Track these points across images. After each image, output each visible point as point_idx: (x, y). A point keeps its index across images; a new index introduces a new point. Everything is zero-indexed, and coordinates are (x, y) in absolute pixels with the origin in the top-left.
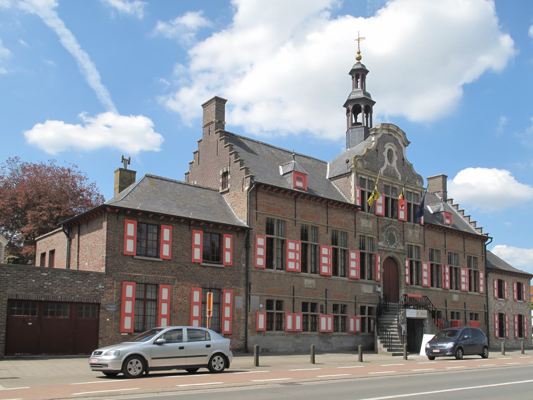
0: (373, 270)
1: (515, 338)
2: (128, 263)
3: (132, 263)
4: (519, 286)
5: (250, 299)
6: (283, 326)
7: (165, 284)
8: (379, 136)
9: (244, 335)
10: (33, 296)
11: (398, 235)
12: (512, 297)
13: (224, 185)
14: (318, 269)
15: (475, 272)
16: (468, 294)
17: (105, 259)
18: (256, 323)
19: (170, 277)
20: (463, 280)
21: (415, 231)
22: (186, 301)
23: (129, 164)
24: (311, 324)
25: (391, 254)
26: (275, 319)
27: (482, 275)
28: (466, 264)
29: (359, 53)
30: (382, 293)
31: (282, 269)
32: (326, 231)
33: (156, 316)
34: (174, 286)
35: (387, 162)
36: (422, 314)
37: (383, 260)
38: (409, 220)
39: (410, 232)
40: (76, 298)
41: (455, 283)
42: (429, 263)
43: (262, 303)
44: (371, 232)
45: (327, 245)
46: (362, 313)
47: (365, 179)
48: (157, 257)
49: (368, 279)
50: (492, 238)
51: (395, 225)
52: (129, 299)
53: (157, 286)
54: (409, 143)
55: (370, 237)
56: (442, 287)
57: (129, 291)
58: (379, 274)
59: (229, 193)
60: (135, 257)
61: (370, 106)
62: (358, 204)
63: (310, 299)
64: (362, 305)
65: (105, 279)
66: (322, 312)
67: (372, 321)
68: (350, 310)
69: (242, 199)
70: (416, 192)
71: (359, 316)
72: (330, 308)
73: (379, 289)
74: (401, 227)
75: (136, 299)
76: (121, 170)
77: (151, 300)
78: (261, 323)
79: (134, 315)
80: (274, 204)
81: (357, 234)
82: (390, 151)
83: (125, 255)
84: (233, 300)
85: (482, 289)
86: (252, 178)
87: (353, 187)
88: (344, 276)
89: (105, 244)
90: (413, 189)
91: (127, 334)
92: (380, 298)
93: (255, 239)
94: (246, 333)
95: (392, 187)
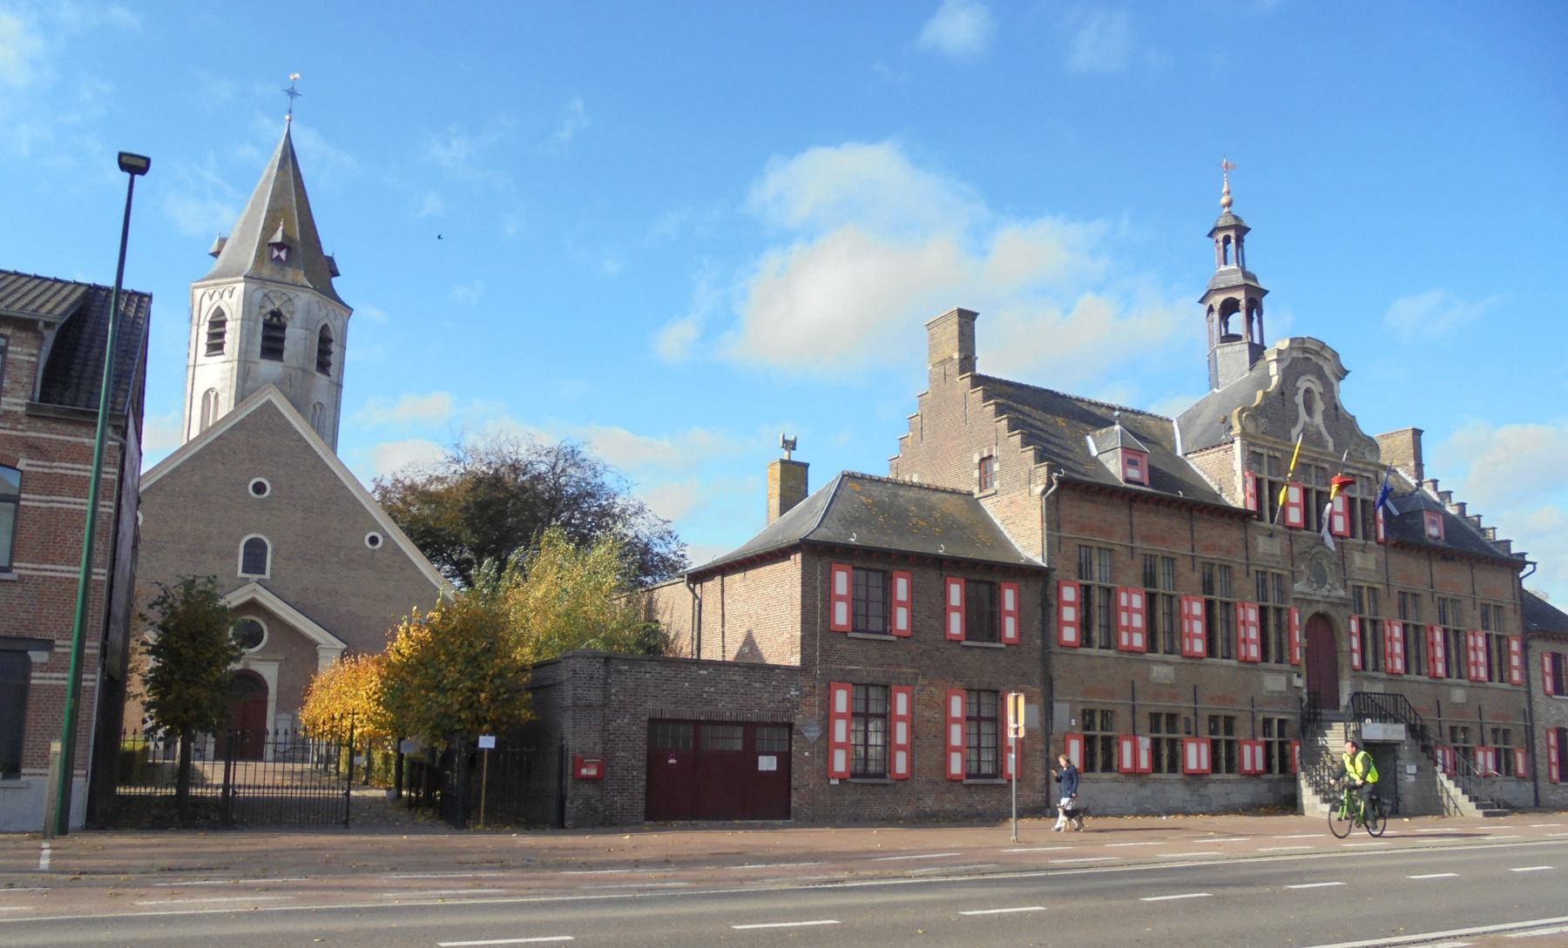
0: (1285, 641)
8: (1286, 363)
10: (686, 714)
14: (1177, 643)
24: (1167, 757)
25: (1321, 608)
27: (1515, 646)
37: (1305, 622)
39: (1358, 559)
42: (1401, 622)
53: (886, 687)
54: (1346, 372)
57: (841, 701)
63: (1165, 705)
66: (1188, 733)
68: (1242, 731)
71: (1261, 739)
76: (783, 462)
77: (877, 716)
81: (1253, 568)
82: (1308, 391)
85: (1516, 676)
87: (1239, 472)
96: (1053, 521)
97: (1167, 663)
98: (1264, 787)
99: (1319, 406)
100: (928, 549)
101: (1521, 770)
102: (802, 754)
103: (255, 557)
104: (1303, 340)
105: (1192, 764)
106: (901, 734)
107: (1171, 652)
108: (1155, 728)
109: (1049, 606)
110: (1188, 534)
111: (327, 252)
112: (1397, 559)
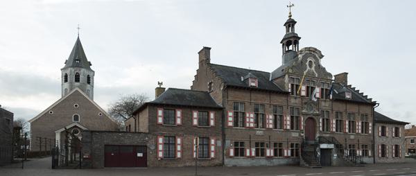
4: (397, 130)
10: (116, 144)
13: (210, 89)
15: (366, 123)
18: (229, 153)
20: (370, 128)
25: (310, 116)
27: (370, 125)
36: (332, 146)
38: (322, 97)
40: (135, 143)
53: (175, 137)
57: (161, 140)
63: (260, 140)
68: (284, 146)
72: (272, 145)
73: (302, 135)
78: (232, 153)
85: (370, 132)
86: (225, 83)
99: (314, 65)
102: (150, 153)
103: (76, 118)
105: (268, 154)
106: (179, 148)
107: (263, 128)
109: (223, 118)
111: (88, 60)
112: (335, 104)
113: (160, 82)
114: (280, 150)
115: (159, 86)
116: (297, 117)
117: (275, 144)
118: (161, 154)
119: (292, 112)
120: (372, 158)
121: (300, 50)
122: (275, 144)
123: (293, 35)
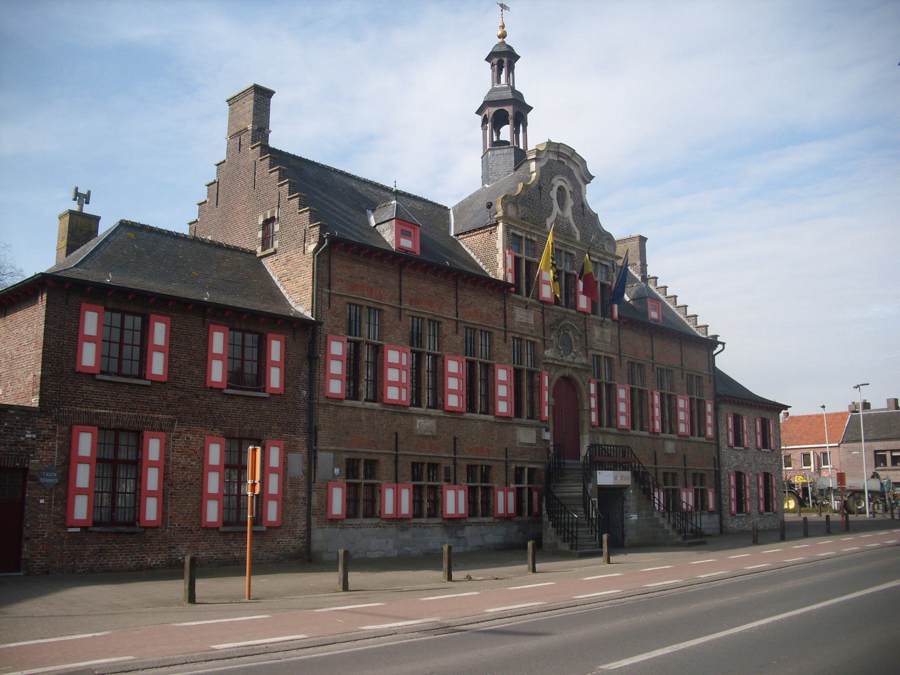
0: (536, 400)
1: (760, 513)
2: (85, 388)
3: (91, 388)
4: (765, 424)
5: (315, 458)
6: (378, 509)
7: (154, 430)
8: (543, 164)
9: (305, 528)
11: (577, 338)
12: (754, 443)
13: (266, 242)
14: (440, 399)
16: (689, 441)
17: (38, 381)
18: (326, 503)
19: (165, 417)
21: (605, 331)
22: (194, 463)
23: (87, 203)
24: (427, 503)
25: (567, 372)
26: (362, 496)
27: (709, 408)
28: (685, 388)
29: (503, 27)
30: (552, 443)
31: (375, 401)
32: (455, 329)
33: (135, 493)
34: (173, 434)
35: (556, 209)
37: (553, 383)
39: (597, 332)
41: (670, 422)
42: (628, 387)
43: (339, 466)
44: (532, 331)
45: (456, 354)
46: (518, 480)
47: (521, 237)
48: (141, 376)
49: (528, 418)
50: (723, 344)
51: (571, 320)
52: (84, 460)
54: (592, 177)
55: (531, 341)
56: (648, 430)
57: (85, 443)
58: (547, 408)
59: (275, 258)
60: (98, 377)
61: (523, 112)
62: (510, 280)
64: (518, 465)
65: (38, 420)
66: (448, 481)
67: (535, 495)
68: (498, 477)
69: (302, 268)
70: (604, 263)
71: (512, 486)
72: (462, 474)
73: (547, 436)
74: (581, 323)
75: (99, 460)
76: (71, 213)
77: (127, 462)
78: (337, 506)
79: (92, 493)
80: (362, 278)
81: (509, 335)
82: (561, 189)
83: (79, 373)
84: (284, 461)
85: (710, 432)
87: (501, 251)
88: (487, 413)
89: (40, 351)
90: (599, 258)
91: (79, 530)
92: (548, 451)
93: (326, 343)
94: (309, 524)
95: (566, 253)
96: (323, 279)
97: (430, 416)
98: (515, 528)
100: (191, 294)
101: (711, 505)
104: (559, 145)
106: (153, 478)
107: (435, 406)
108: (416, 477)
110: (453, 301)
113: (83, 191)
114: (487, 490)
115: (75, 207)
116: (531, 373)
117: (414, 465)
118: (81, 509)
119: (518, 356)
120: (716, 517)
121: (531, 147)
122: (471, 469)
123: (509, 95)
